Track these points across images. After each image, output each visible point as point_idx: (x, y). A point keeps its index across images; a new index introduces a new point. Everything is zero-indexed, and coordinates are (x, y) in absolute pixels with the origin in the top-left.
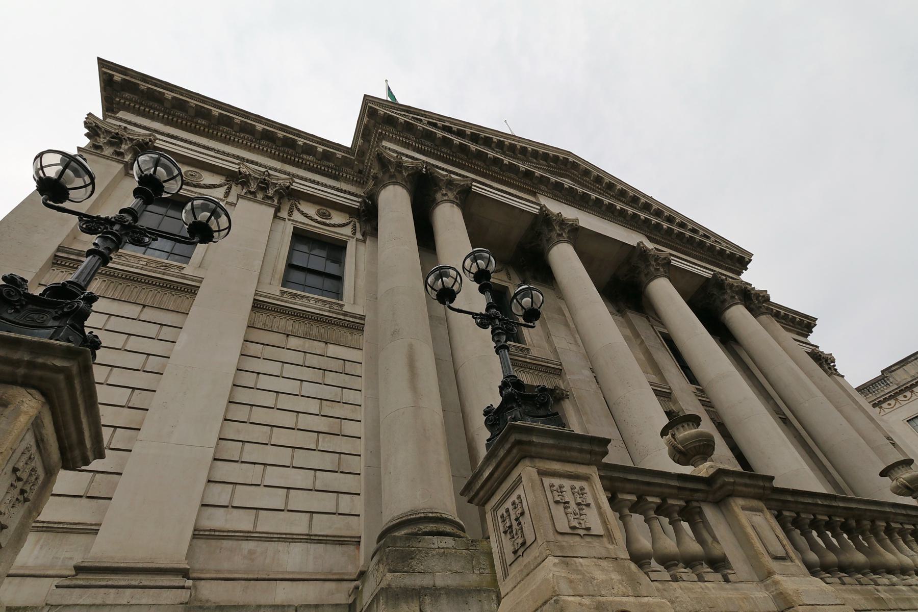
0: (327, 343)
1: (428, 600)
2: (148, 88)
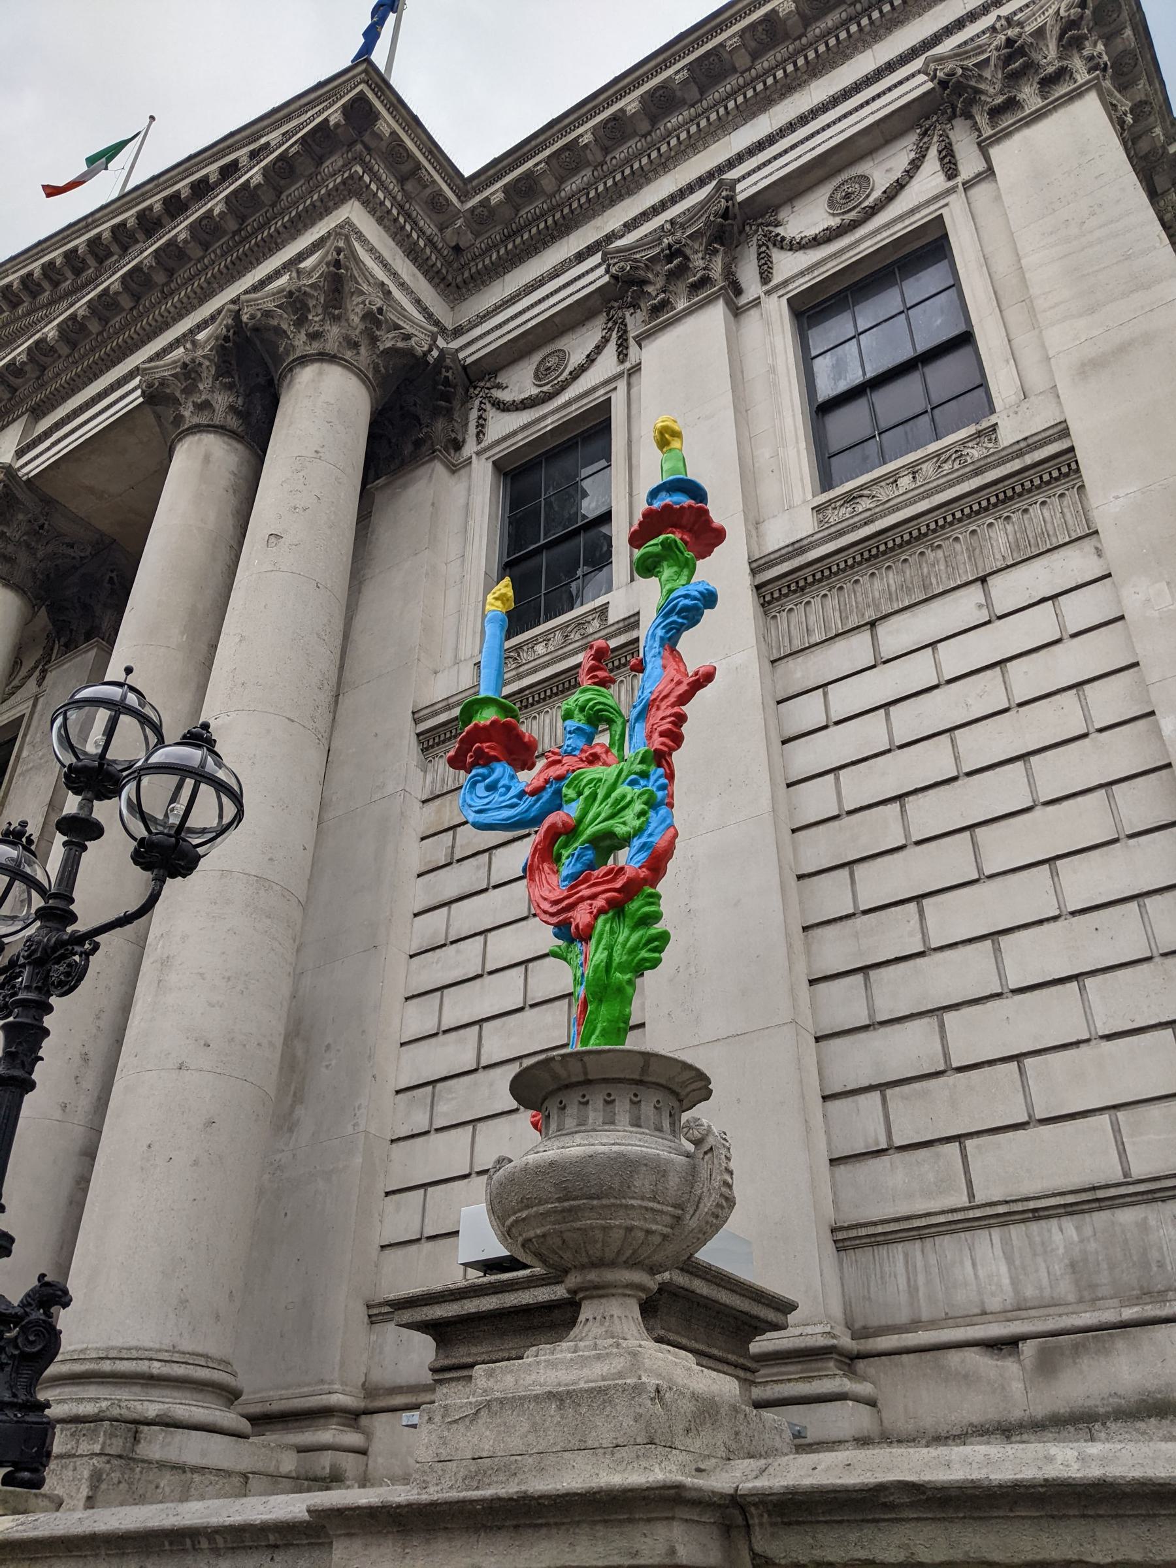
2: (690, 67)
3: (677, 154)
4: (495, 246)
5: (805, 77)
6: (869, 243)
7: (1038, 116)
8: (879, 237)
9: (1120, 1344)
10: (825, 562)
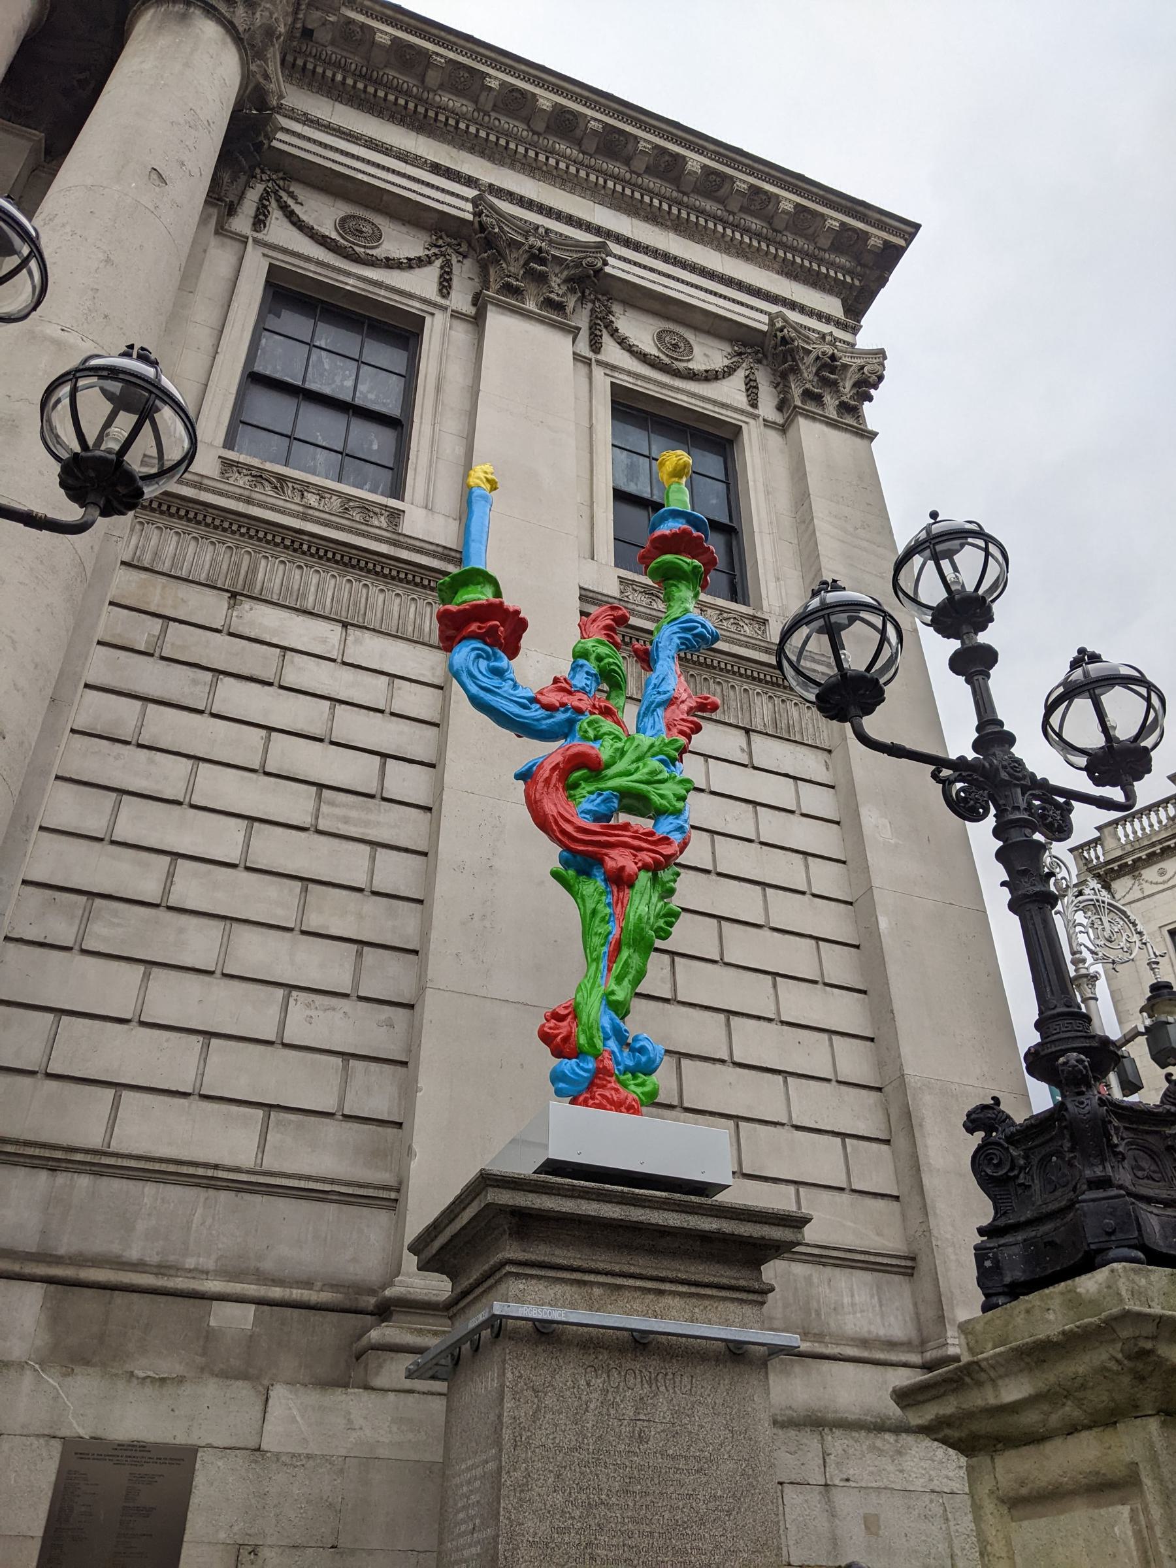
0: (345, 625)
1: (827, 1430)
2: (395, 40)
3: (547, 172)
4: (345, 69)
5: (669, 223)
6: (685, 398)
7: (527, 315)
8: (693, 401)
9: (797, 1369)
10: (637, 633)
